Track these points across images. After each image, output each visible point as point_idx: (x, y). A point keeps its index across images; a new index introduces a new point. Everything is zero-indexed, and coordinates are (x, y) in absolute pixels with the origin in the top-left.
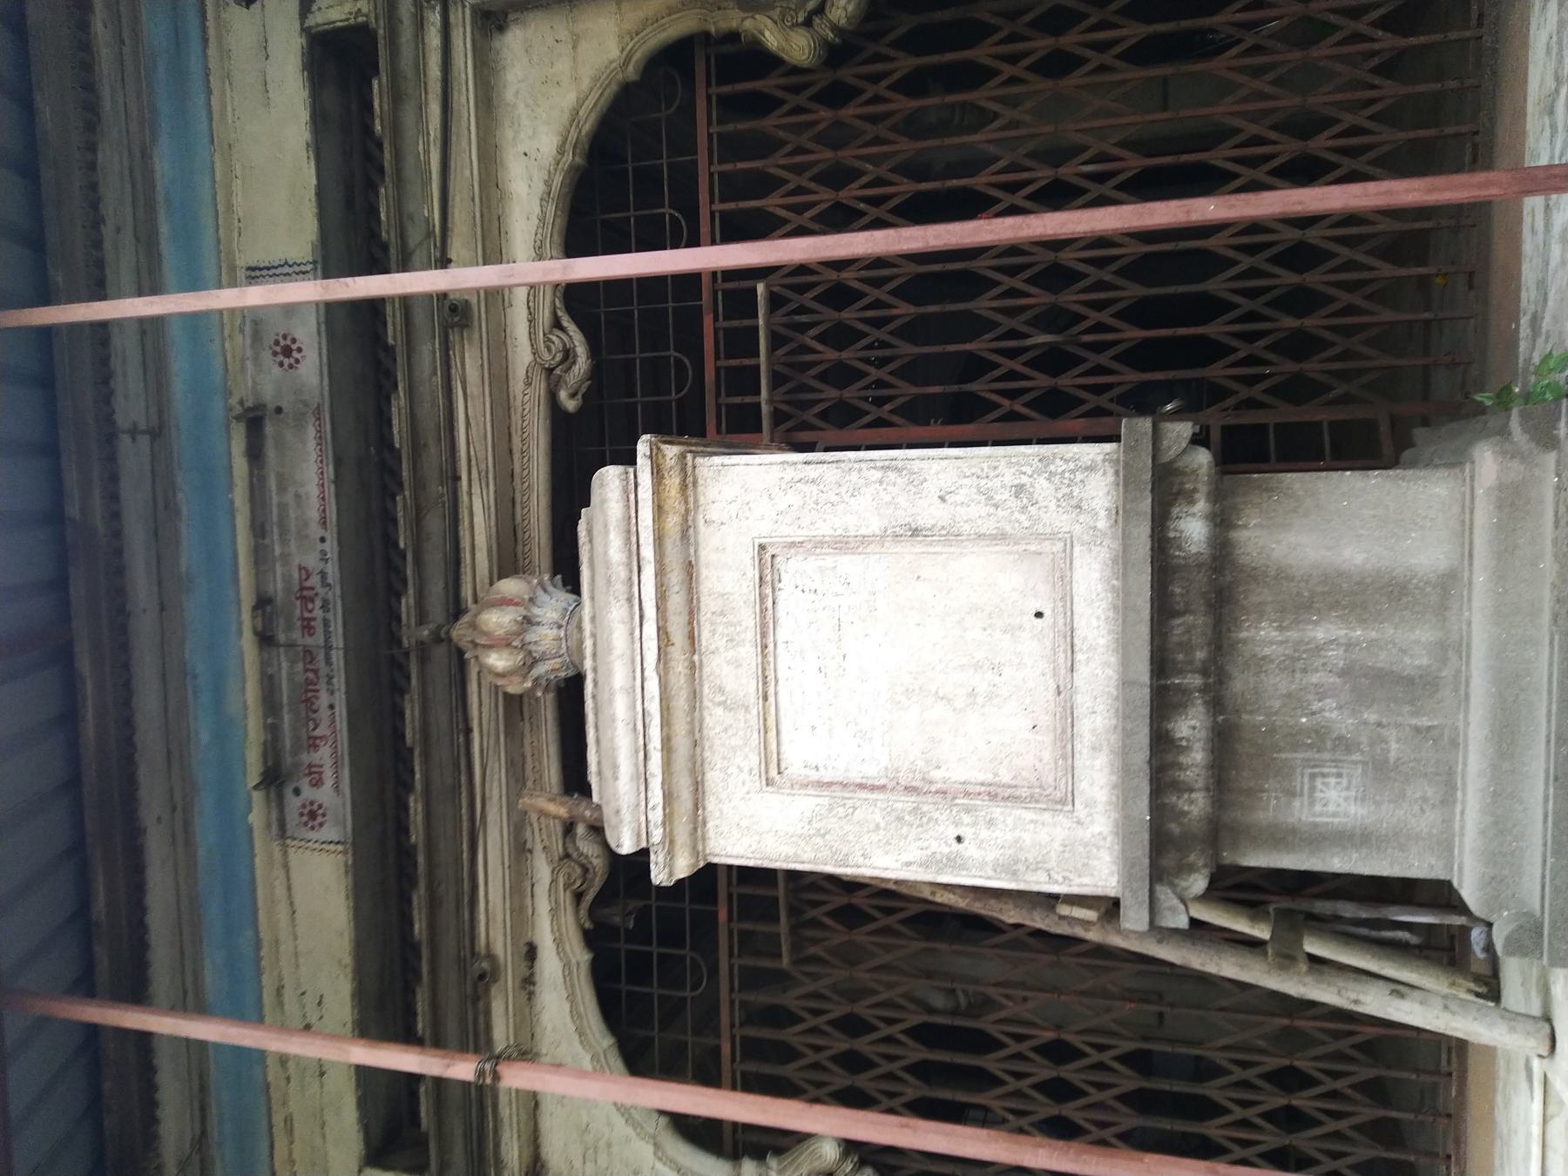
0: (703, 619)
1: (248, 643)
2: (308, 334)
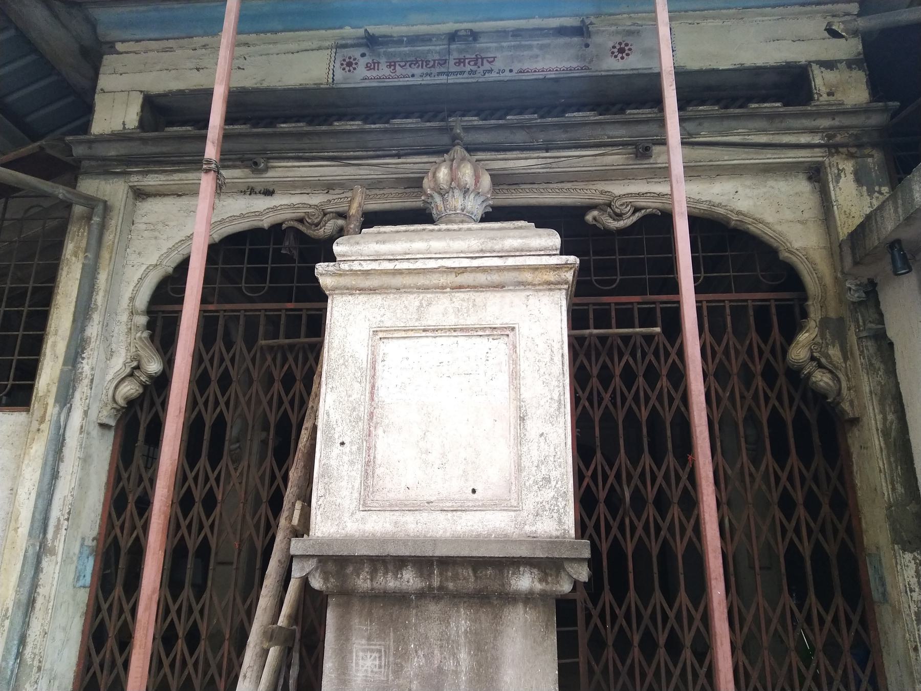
0: (471, 294)
1: (449, 27)
2: (634, 63)
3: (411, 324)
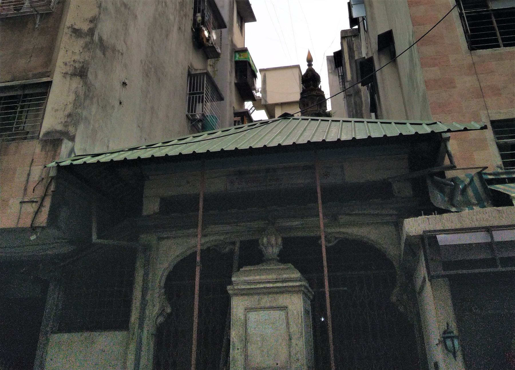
3: (256, 306)
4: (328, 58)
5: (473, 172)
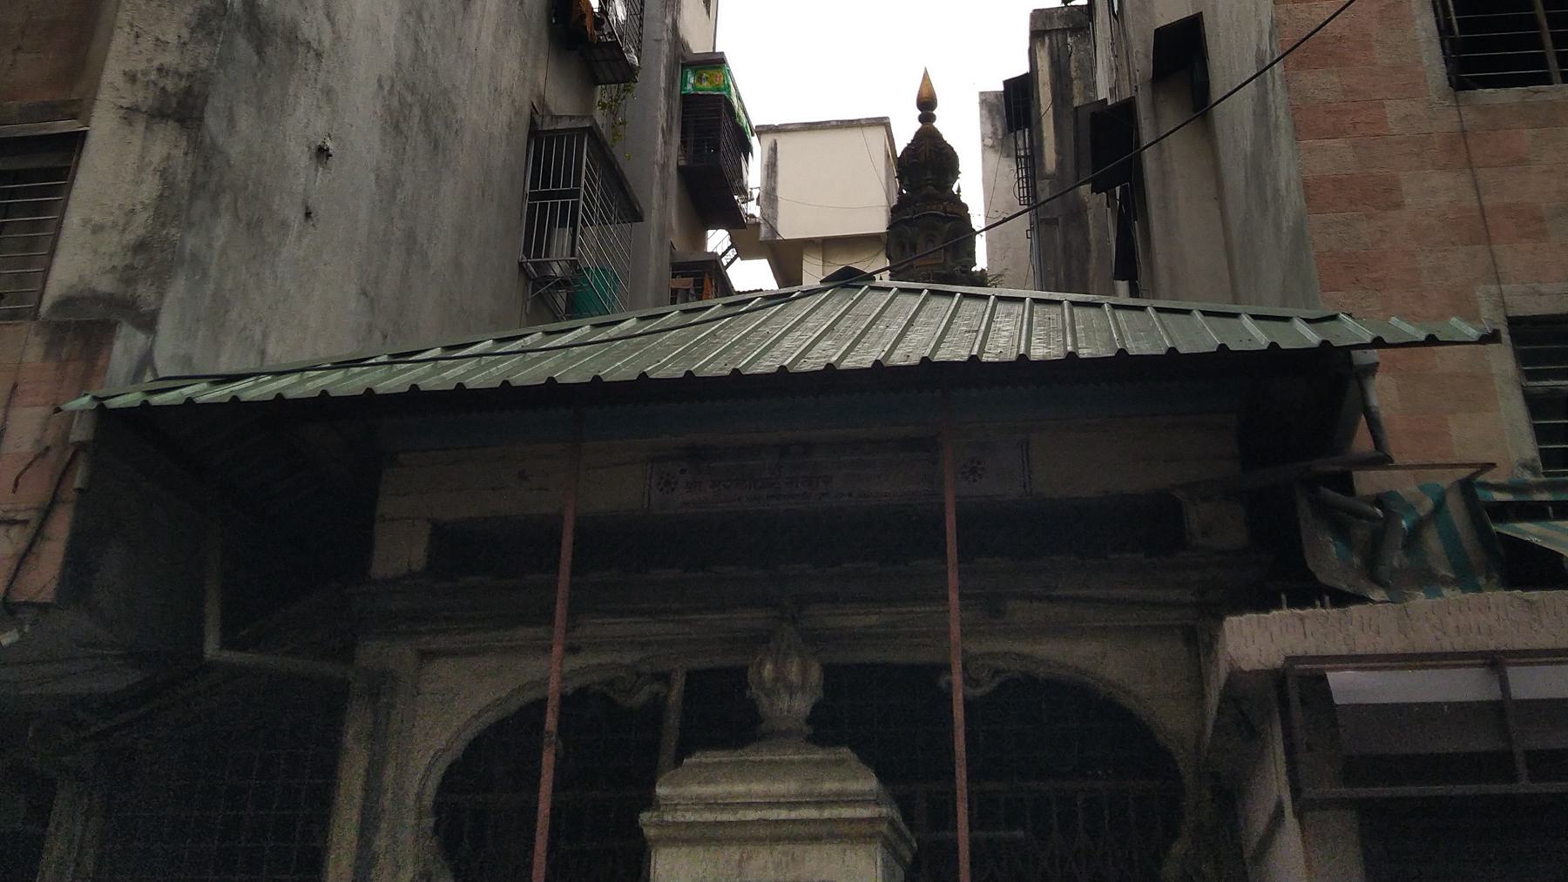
4: (986, 101)
5: (1446, 480)
